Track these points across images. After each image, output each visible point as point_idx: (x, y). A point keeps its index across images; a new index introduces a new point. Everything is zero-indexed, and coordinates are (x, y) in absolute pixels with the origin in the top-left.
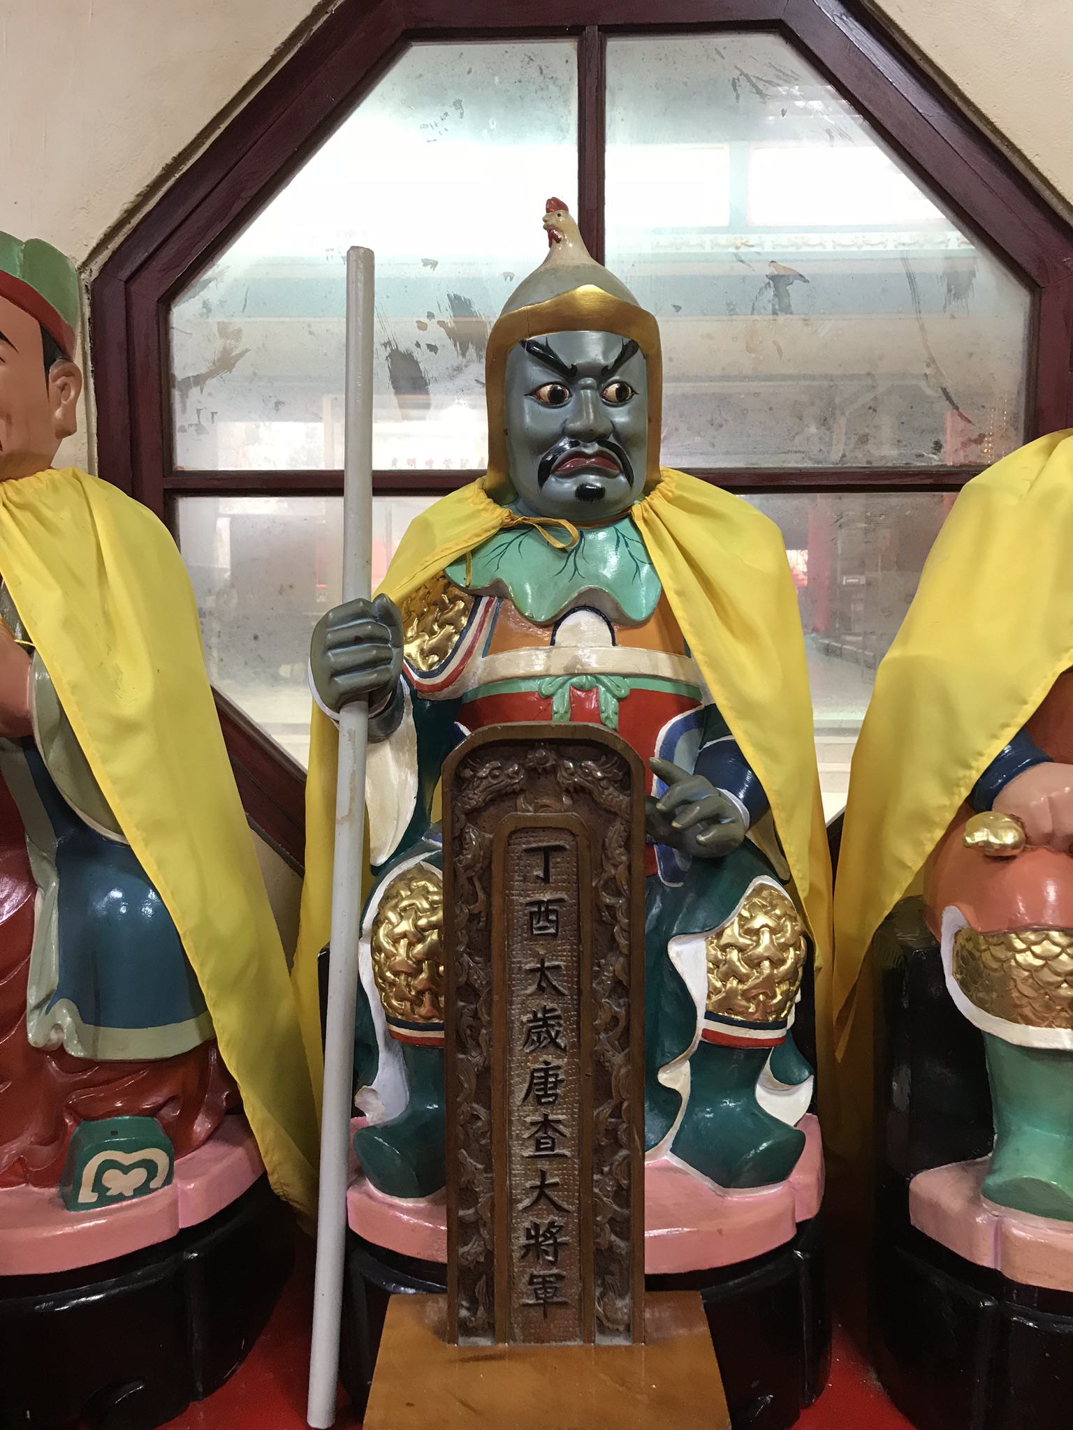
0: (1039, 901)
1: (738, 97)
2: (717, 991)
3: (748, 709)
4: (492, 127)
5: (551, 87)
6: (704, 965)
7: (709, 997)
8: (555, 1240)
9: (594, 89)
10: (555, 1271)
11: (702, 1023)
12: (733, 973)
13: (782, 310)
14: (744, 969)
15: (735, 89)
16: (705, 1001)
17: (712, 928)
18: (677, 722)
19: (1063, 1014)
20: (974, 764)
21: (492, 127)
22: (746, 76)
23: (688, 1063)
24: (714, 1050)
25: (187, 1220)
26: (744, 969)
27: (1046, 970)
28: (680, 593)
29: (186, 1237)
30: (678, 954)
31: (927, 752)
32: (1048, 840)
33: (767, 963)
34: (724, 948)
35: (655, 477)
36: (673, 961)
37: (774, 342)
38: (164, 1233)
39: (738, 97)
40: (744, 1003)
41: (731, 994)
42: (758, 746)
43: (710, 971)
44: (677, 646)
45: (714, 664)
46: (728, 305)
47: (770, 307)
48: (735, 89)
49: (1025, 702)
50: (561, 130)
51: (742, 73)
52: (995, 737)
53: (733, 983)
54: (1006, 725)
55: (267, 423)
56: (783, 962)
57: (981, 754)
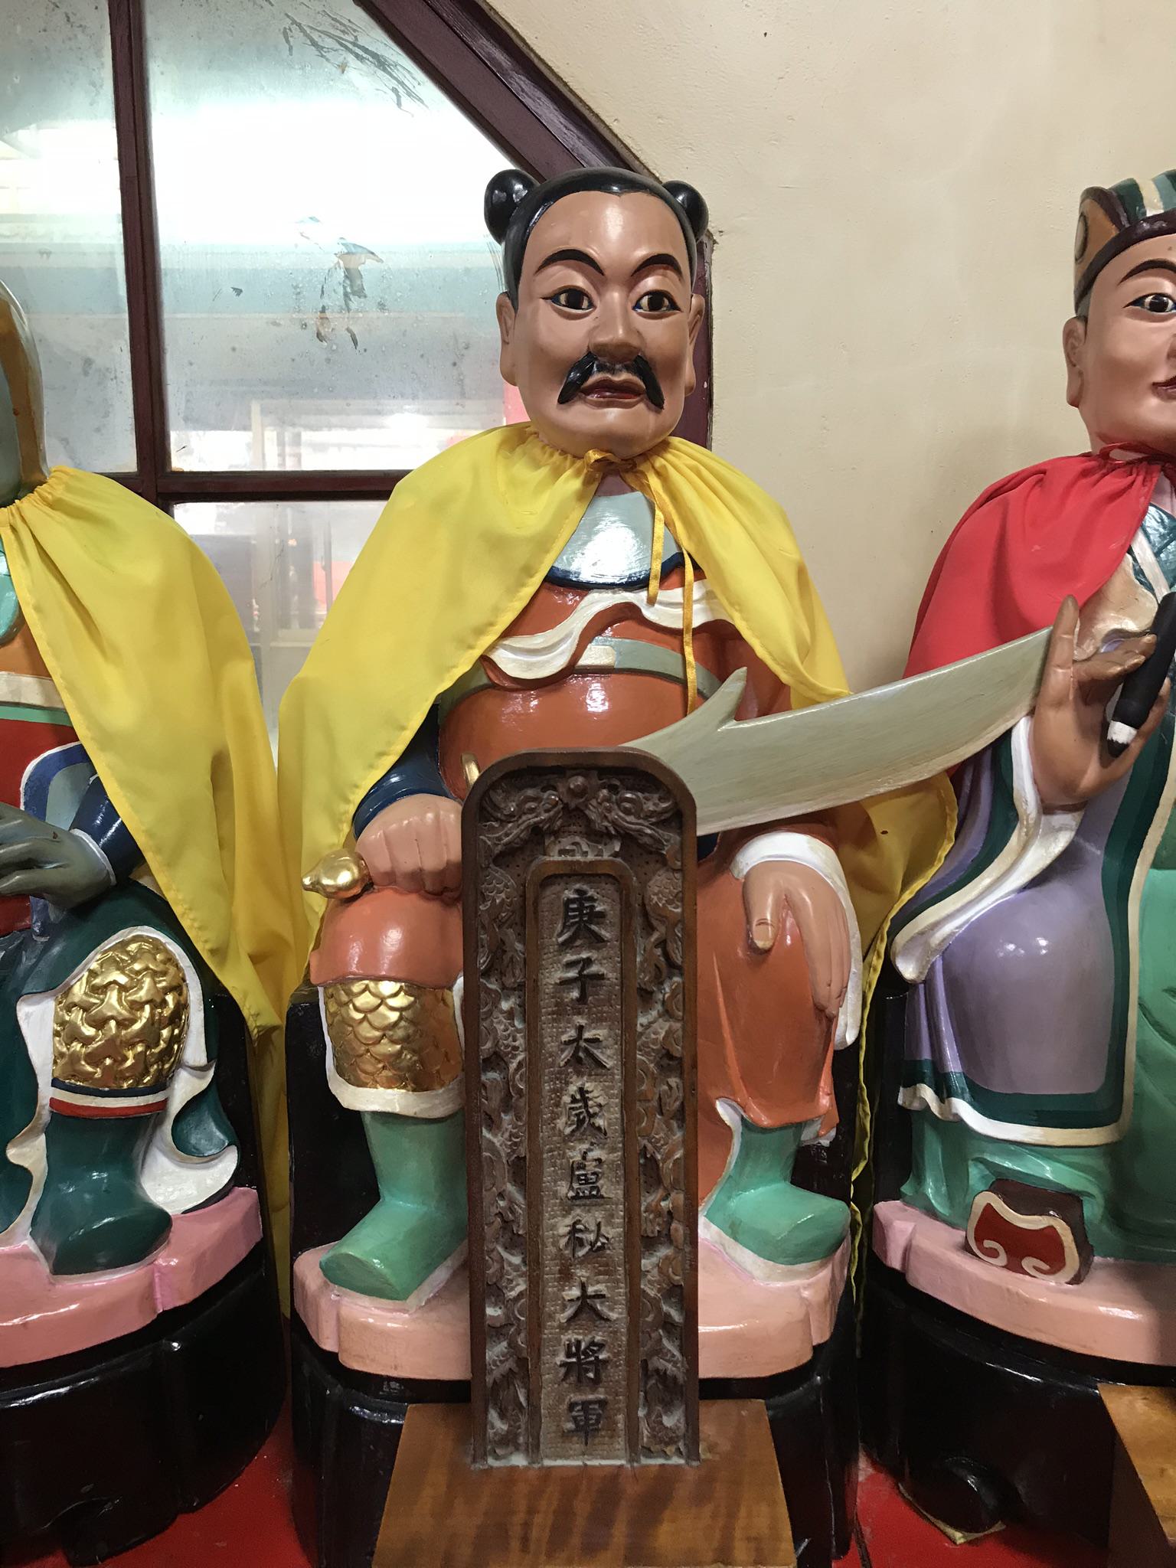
0: (372, 950)
1: (291, 48)
2: (62, 1055)
3: (108, 740)
4: (17, 81)
5: (80, 36)
6: (51, 1026)
7: (55, 1062)
9: (125, 39)
11: (47, 1092)
12: (74, 1035)
13: (354, 293)
14: (88, 1031)
15: (288, 41)
16: (50, 1067)
17: (55, 983)
18: (50, 756)
19: (385, 1073)
20: (351, 797)
21: (17, 81)
22: (299, 25)
23: (43, 1137)
24: (65, 1121)
25: (166, 1301)
26: (88, 1031)
27: (365, 1024)
28: (38, 609)
29: (168, 1322)
30: (28, 1016)
31: (316, 787)
32: (391, 878)
33: (113, 1023)
34: (69, 1010)
35: (37, 477)
36: (21, 1023)
37: (348, 330)
38: (133, 1322)
39: (291, 48)
40: (89, 1069)
41: (74, 1058)
42: (124, 783)
43: (56, 1034)
44: (39, 670)
45: (72, 689)
46: (296, 287)
47: (341, 290)
48: (288, 41)
49: (403, 728)
50: (93, 84)
51: (294, 22)
52: (371, 766)
53: (77, 1046)
54: (382, 754)
55: (201, 433)
56: (134, 1021)
57: (356, 786)
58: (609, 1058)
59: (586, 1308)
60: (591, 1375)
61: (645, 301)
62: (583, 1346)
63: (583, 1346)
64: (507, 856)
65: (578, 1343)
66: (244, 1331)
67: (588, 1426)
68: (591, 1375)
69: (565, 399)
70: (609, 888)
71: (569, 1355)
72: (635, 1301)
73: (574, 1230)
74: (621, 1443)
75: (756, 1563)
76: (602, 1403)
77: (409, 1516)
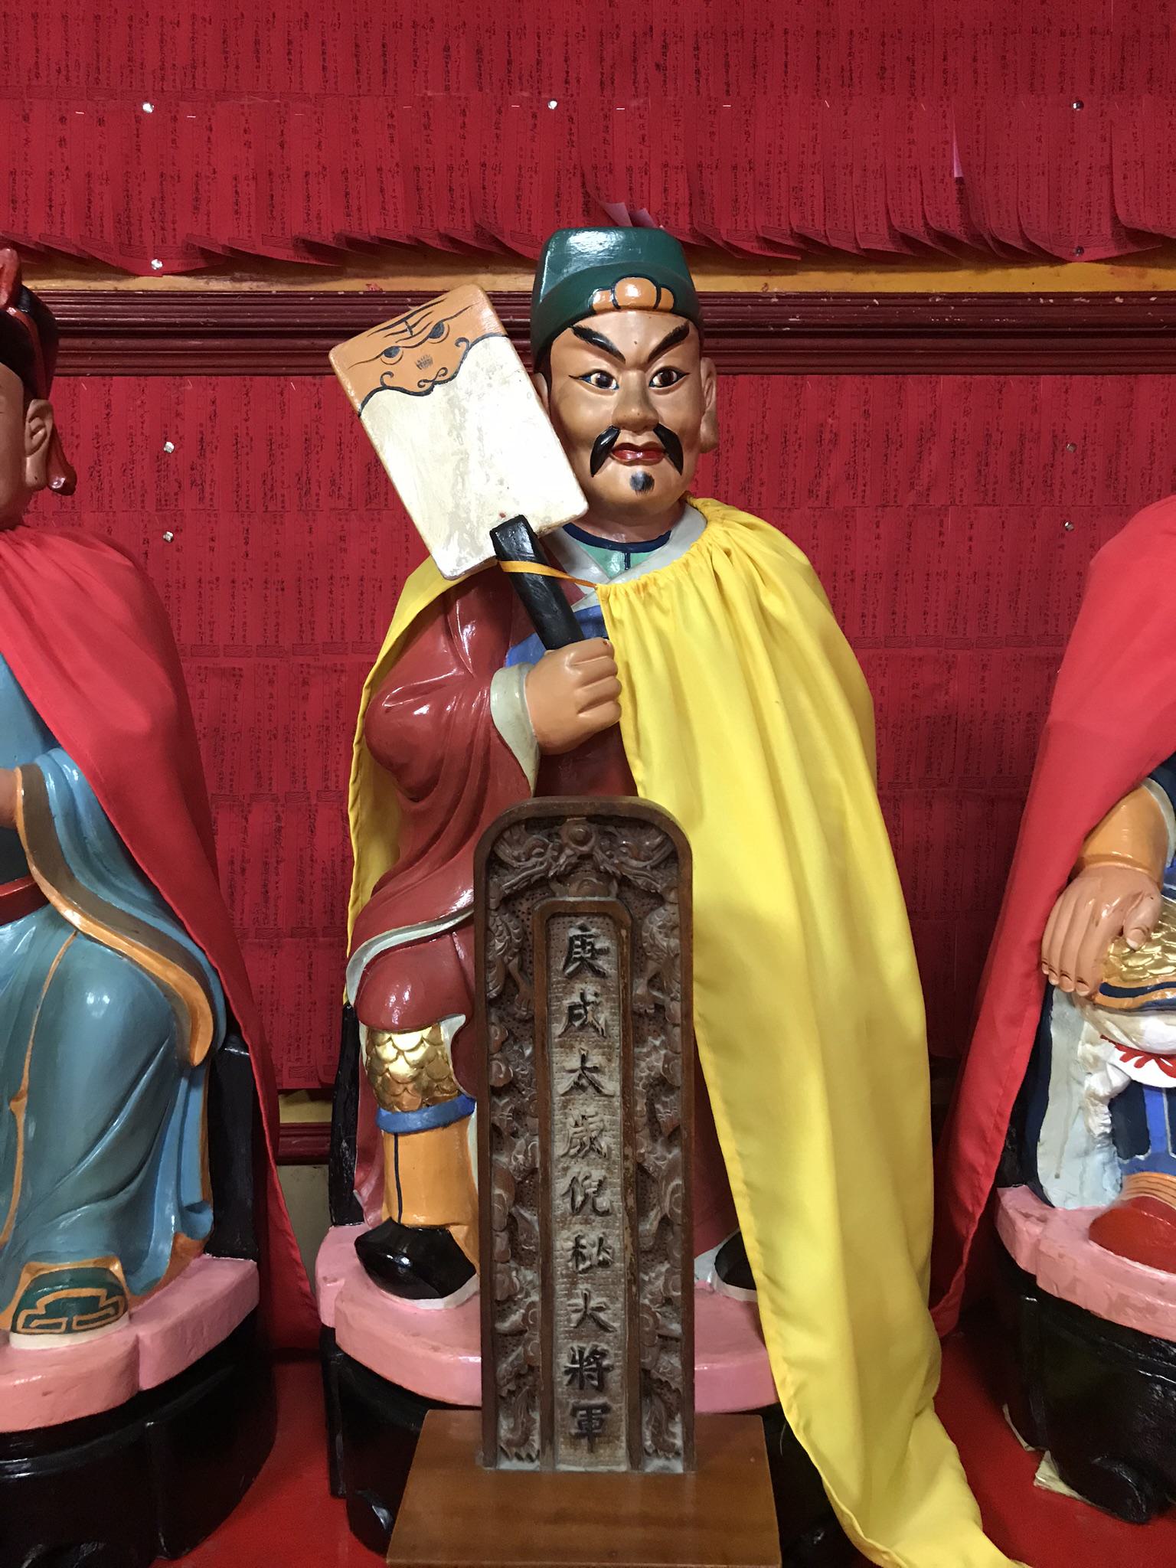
8: (599, 1365)
10: (600, 1400)
58: (612, 1085)
59: (589, 1317)
60: (596, 1383)
61: (656, 380)
62: (586, 1354)
63: (586, 1354)
64: (508, 901)
65: (581, 1353)
66: (270, 1354)
67: (592, 1431)
68: (596, 1383)
69: (137, 1340)
70: (556, 928)
71: (573, 1362)
72: (633, 1309)
73: (578, 1245)
74: (622, 1452)
75: (52, 410)
76: (605, 1408)
77: (427, 1501)
